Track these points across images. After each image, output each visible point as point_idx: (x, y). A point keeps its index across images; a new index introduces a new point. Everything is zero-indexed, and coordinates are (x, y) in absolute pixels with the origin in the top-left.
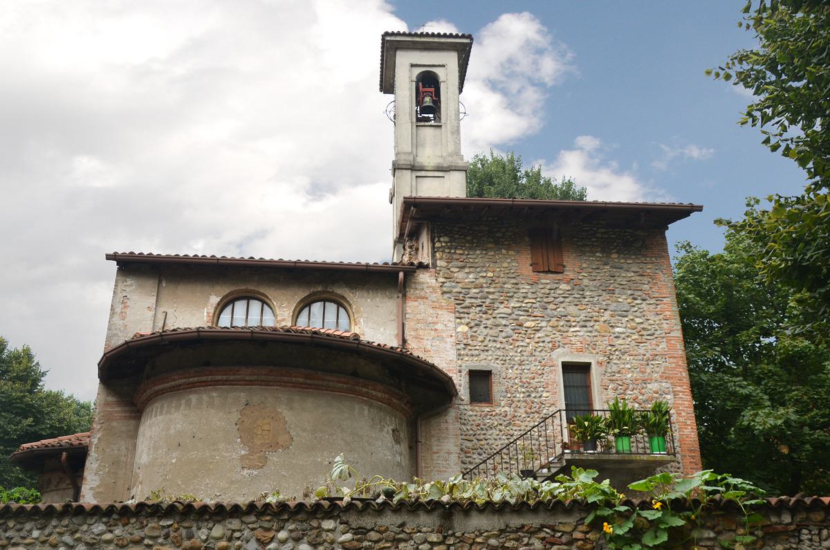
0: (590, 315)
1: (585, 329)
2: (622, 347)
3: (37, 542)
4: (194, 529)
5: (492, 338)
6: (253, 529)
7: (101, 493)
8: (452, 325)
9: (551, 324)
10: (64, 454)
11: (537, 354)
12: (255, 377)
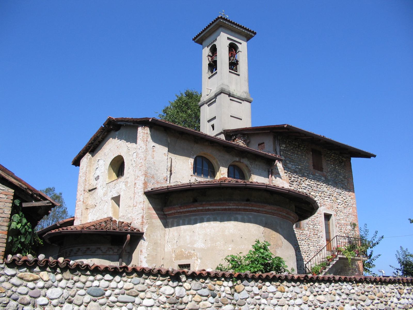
0: (331, 193)
2: (340, 209)
3: (327, 293)
4: (379, 288)
7: (149, 260)
10: (129, 236)
12: (270, 211)
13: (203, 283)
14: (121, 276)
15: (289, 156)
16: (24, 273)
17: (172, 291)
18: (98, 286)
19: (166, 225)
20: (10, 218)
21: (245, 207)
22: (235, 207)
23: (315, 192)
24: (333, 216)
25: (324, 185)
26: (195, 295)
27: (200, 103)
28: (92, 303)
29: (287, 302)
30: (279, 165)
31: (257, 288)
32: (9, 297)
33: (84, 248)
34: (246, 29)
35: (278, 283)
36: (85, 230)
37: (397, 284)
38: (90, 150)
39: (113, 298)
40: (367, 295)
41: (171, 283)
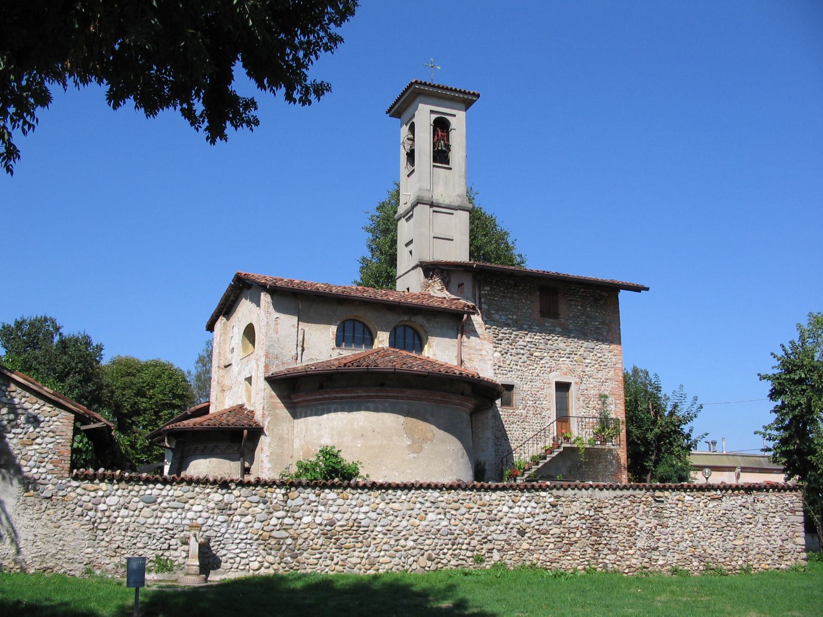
0: (572, 350)
1: (569, 359)
4: (482, 496)
5: (515, 363)
6: (510, 496)
7: (273, 459)
8: (491, 352)
9: (549, 354)
10: (246, 431)
11: (540, 375)
12: (414, 396)
13: (253, 490)
14: (171, 485)
15: (495, 302)
16: (86, 484)
17: (221, 498)
18: (151, 494)
19: (295, 416)
20: (73, 439)
21: (378, 394)
22: (365, 394)
24: (573, 385)
25: (561, 338)
26: (245, 501)
27: (396, 216)
28: (145, 509)
29: (350, 510)
30: (477, 319)
31: (314, 495)
32: (76, 504)
33: (201, 447)
35: (340, 491)
36: (198, 426)
37: (510, 491)
38: (223, 313)
39: (164, 505)
40: (462, 504)
41: (220, 491)
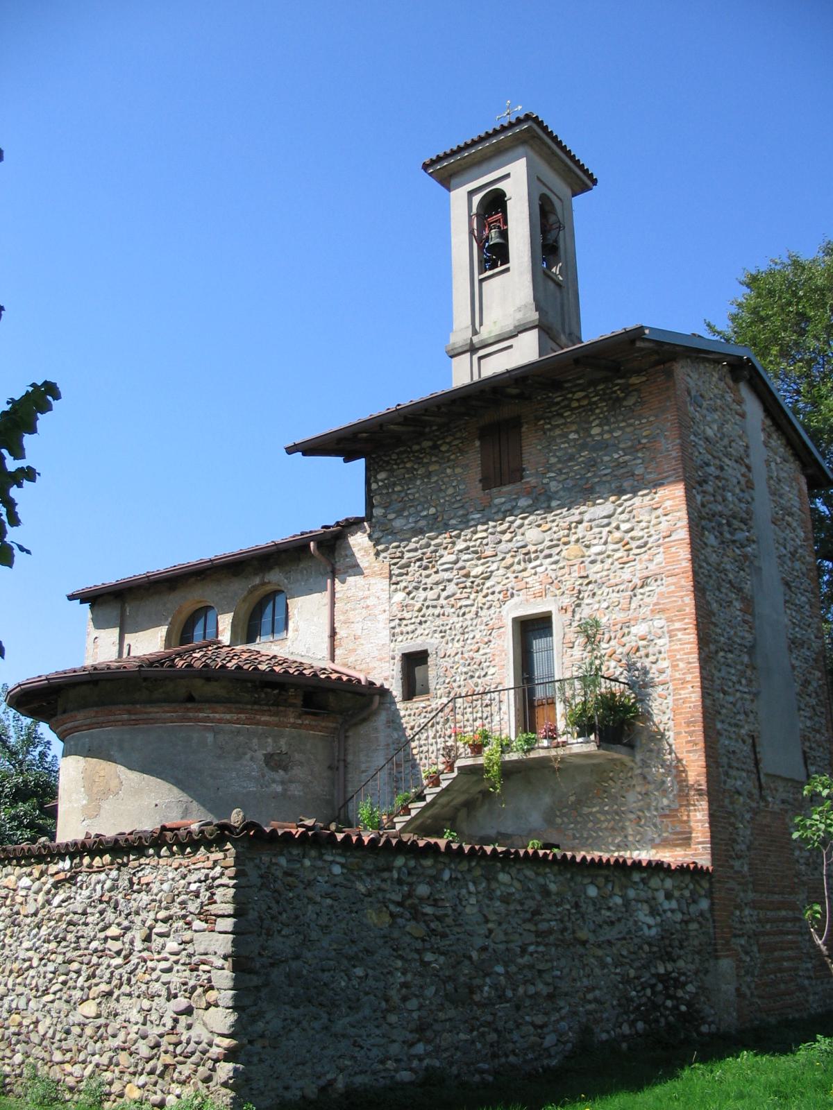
23: (487, 562)
34: (496, 132)
